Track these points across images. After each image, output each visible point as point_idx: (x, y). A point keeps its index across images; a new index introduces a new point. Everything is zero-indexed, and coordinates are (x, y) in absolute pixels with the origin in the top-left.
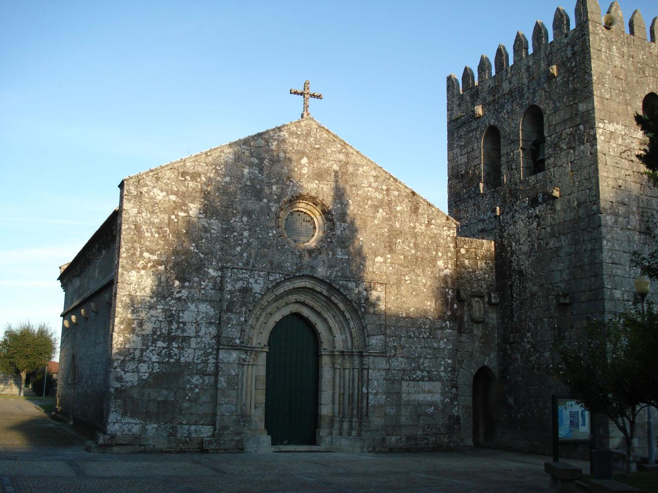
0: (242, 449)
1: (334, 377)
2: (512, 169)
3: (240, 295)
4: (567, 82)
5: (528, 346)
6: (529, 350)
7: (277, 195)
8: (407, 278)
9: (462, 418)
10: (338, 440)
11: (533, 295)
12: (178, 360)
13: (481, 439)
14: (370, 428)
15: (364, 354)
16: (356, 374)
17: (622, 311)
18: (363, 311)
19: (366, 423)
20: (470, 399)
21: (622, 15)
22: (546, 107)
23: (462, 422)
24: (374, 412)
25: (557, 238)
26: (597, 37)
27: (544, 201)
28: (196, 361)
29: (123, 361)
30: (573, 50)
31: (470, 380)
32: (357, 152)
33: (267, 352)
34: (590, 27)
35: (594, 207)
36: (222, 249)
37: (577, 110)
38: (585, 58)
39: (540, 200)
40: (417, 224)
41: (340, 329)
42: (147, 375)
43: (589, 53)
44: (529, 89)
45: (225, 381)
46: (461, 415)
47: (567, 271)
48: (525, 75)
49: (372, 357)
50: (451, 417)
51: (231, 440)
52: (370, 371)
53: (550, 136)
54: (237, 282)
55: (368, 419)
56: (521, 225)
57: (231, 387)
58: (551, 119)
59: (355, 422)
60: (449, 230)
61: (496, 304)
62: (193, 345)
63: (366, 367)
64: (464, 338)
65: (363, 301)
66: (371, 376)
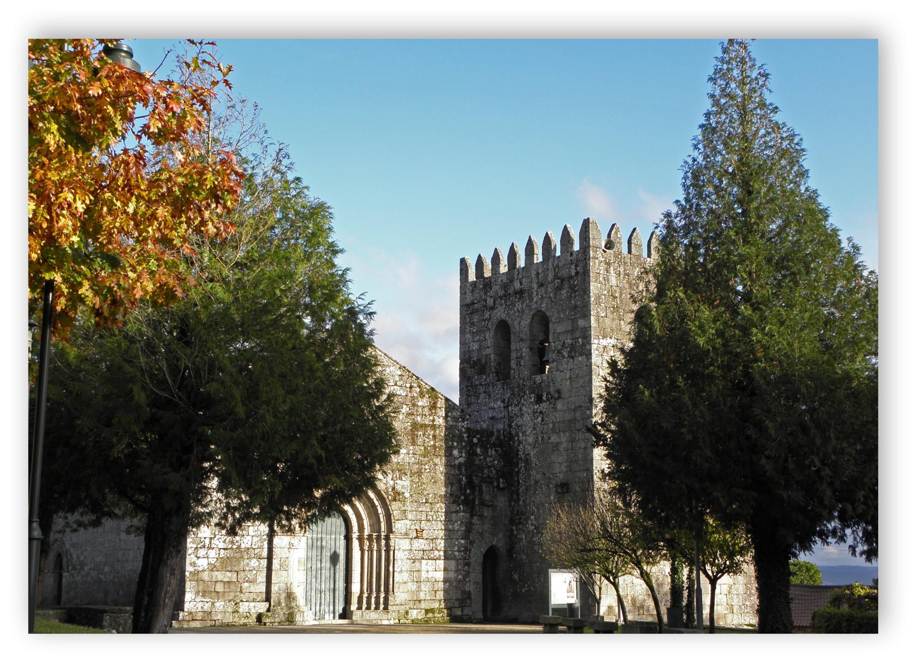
0: (292, 622)
2: (521, 365)
4: (571, 297)
5: (532, 528)
6: (533, 531)
8: (427, 467)
9: (473, 593)
11: (536, 482)
12: (239, 547)
13: (489, 613)
20: (481, 576)
21: (623, 236)
22: (553, 315)
23: (473, 597)
25: (557, 433)
26: (597, 261)
27: (548, 400)
28: (254, 547)
29: (197, 548)
30: (576, 269)
31: (481, 560)
32: (385, 354)
34: (591, 252)
35: (588, 412)
37: (577, 324)
38: (585, 280)
39: (544, 398)
40: (435, 417)
42: (215, 560)
43: (589, 276)
44: (537, 294)
46: (472, 591)
47: (565, 464)
48: (535, 280)
50: (464, 592)
53: (554, 342)
56: (527, 418)
58: (556, 328)
60: (463, 421)
61: (503, 489)
62: (251, 533)
64: (475, 520)
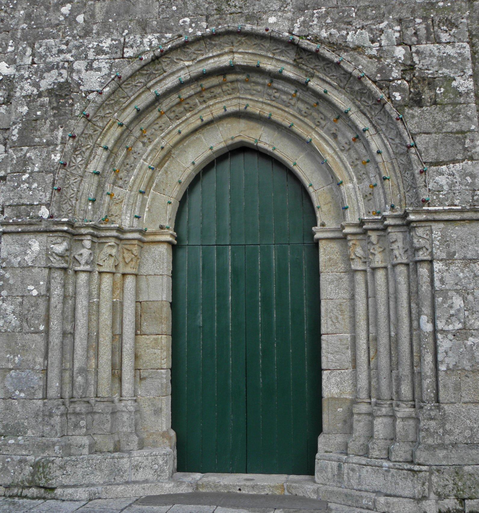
1: (353, 297)
3: (50, 102)
7: (393, 77)
10: (353, 470)
14: (448, 439)
15: (412, 217)
16: (402, 280)
17: (449, 442)
18: (398, 98)
19: (433, 423)
24: (457, 388)
33: (169, 243)
36: (28, 17)
41: (354, 166)
45: (13, 312)
49: (441, 225)
51: (20, 461)
52: (437, 266)
54: (45, 75)
55: (438, 408)
57: (30, 327)
59: (403, 419)
63: (422, 255)
65: (396, 73)
66: (442, 281)
